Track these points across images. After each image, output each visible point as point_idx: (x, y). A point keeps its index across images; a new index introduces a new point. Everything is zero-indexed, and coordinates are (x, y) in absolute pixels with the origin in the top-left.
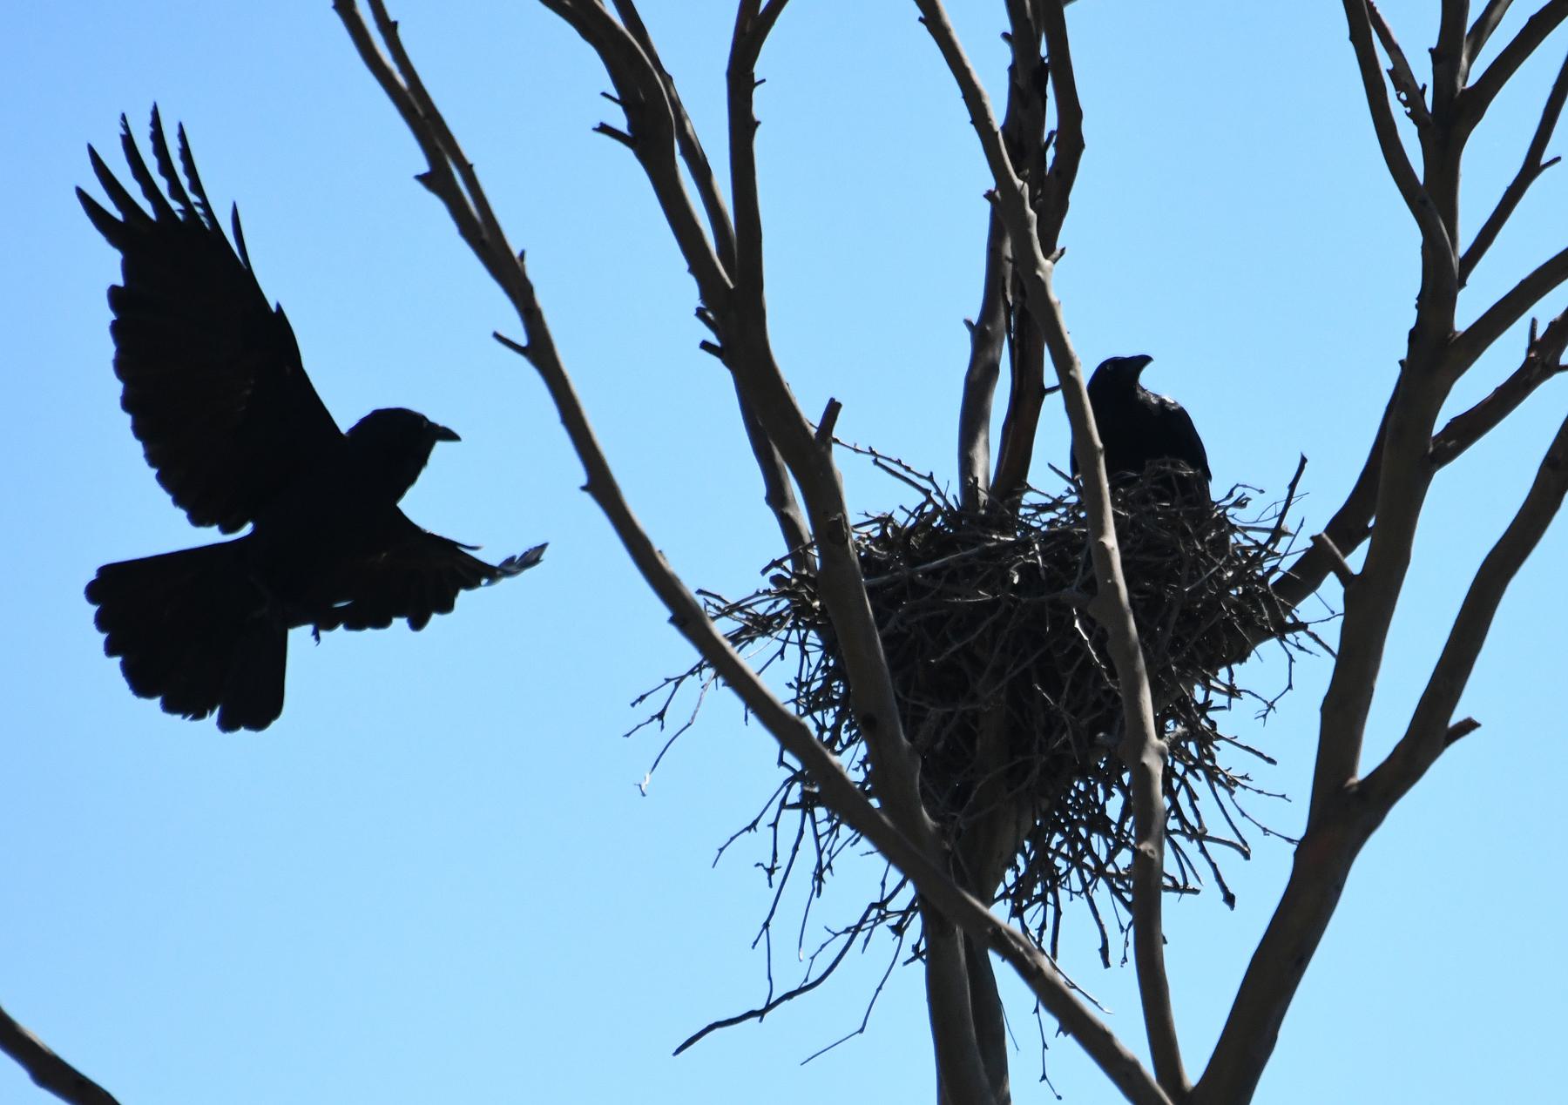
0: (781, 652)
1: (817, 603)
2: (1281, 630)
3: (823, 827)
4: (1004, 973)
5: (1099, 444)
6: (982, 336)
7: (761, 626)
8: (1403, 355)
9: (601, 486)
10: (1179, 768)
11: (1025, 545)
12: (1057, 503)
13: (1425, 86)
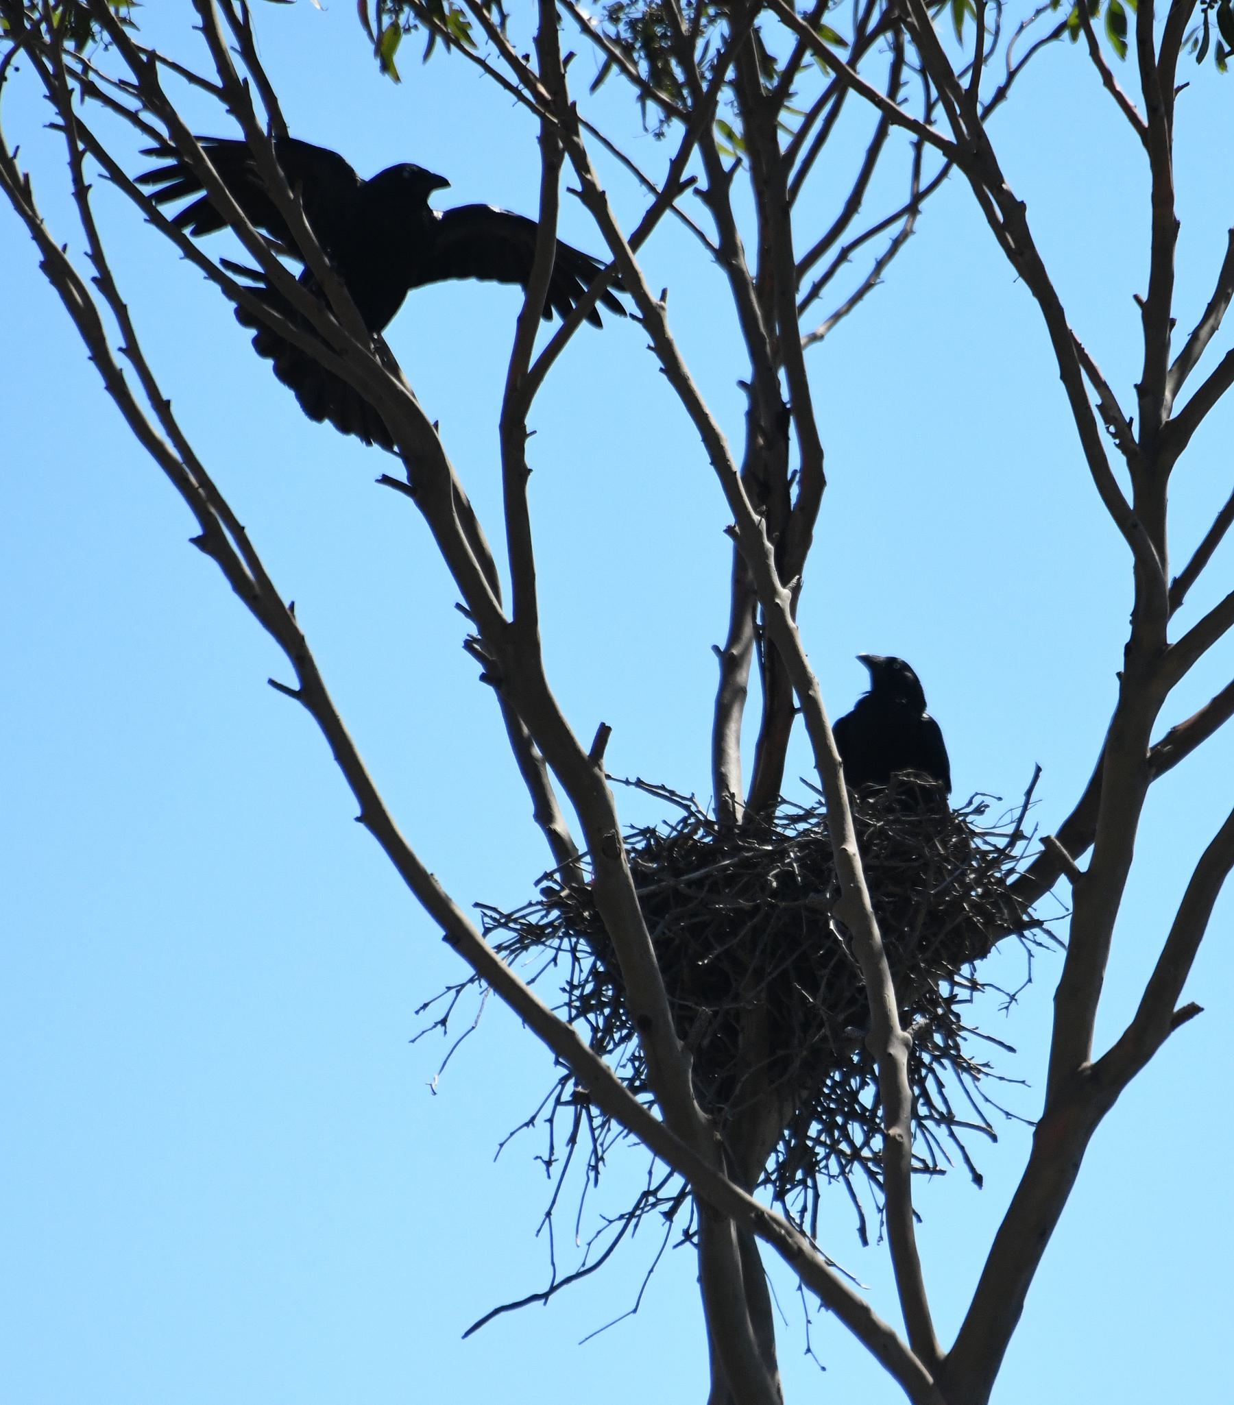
0: (555, 960)
1: (586, 914)
2: (1019, 928)
3: (597, 1122)
4: (767, 1253)
5: (839, 759)
6: (730, 663)
7: (532, 935)
8: (1121, 668)
9: (374, 816)
10: (926, 1058)
11: (781, 854)
12: (809, 814)
13: (1131, 419)
